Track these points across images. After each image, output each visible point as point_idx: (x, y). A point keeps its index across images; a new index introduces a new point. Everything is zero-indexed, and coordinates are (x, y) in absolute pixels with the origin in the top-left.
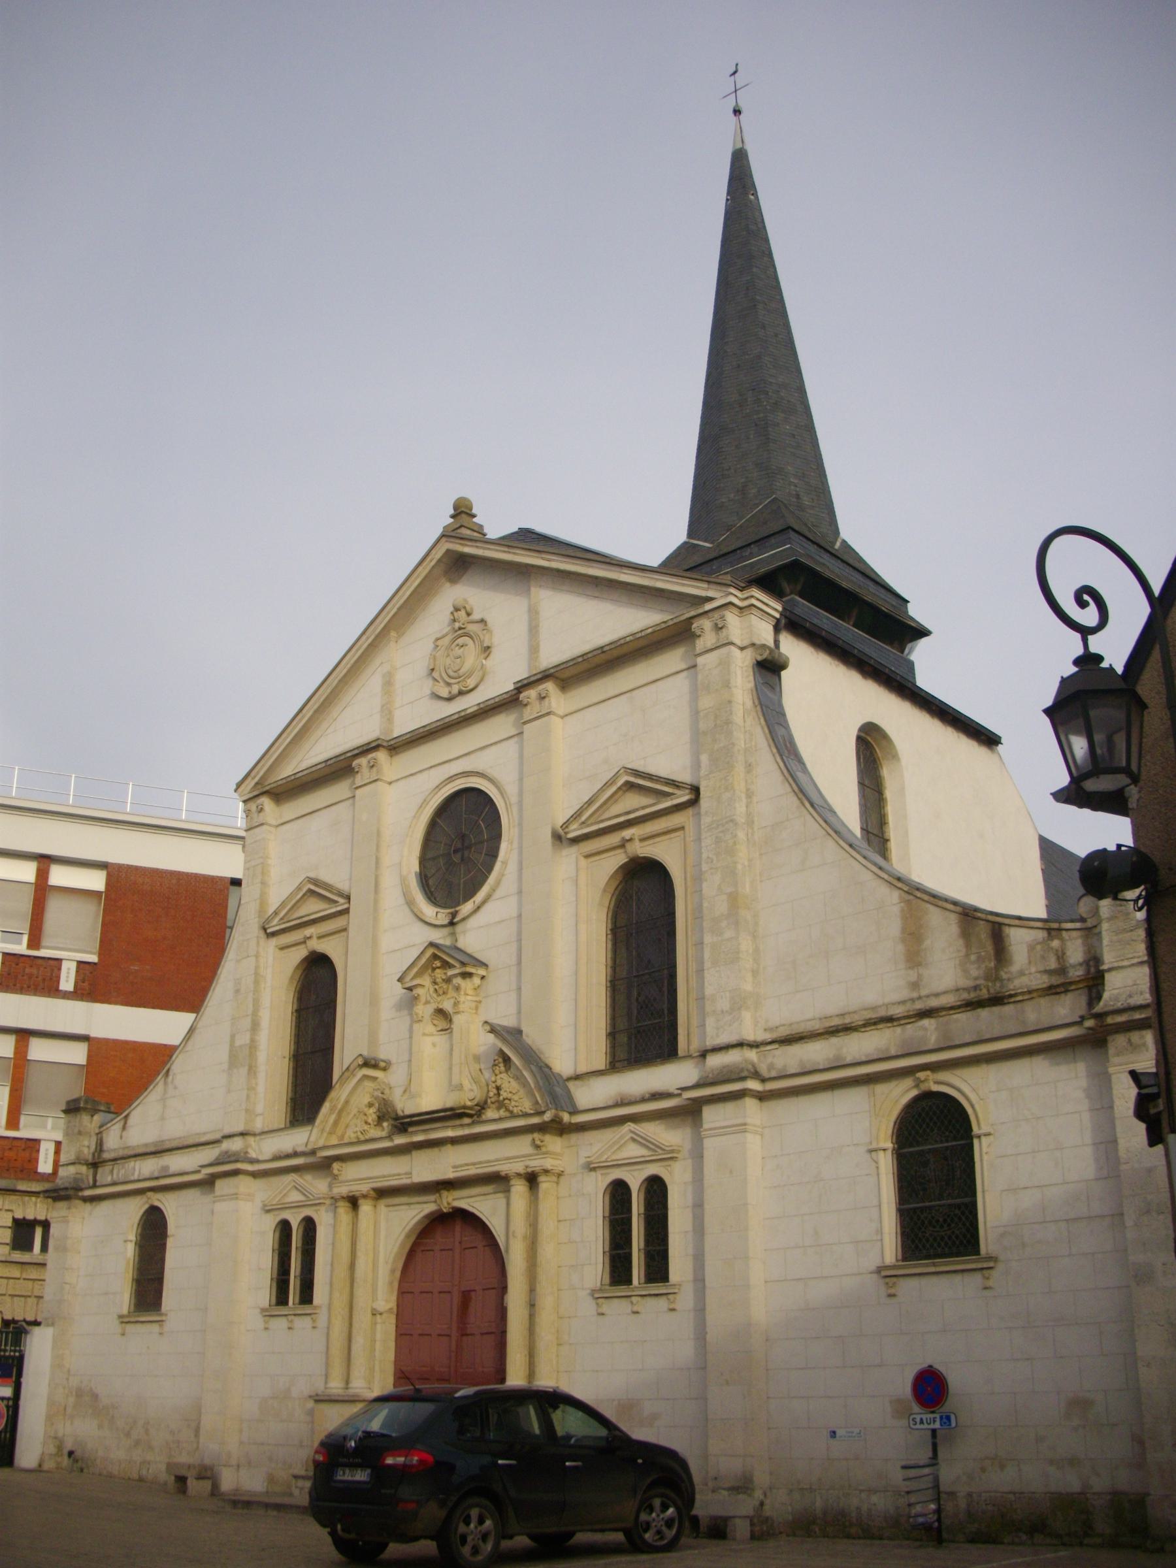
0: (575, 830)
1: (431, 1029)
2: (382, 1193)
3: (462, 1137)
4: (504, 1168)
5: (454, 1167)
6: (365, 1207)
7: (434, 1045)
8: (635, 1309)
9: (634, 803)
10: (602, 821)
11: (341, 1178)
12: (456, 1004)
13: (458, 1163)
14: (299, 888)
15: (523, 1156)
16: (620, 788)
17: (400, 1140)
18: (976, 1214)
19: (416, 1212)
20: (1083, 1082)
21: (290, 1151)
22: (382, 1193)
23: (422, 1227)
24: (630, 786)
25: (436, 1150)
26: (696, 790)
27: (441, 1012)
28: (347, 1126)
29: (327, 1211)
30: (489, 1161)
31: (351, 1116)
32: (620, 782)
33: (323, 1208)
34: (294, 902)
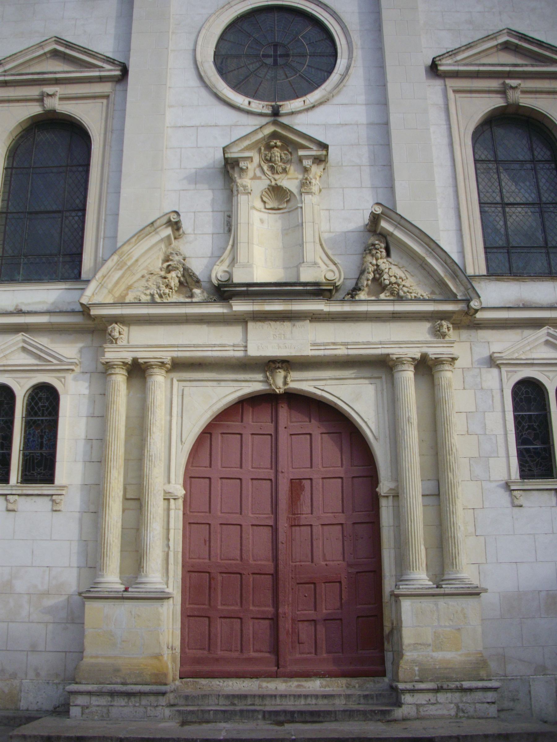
0: (450, 65)
1: (259, 204)
2: (178, 366)
3: (329, 313)
4: (395, 352)
5: (314, 344)
6: (159, 380)
7: (262, 221)
8: (11, 507)
9: (507, 59)
10: (484, 65)
11: (119, 342)
12: (305, 184)
13: (318, 341)
14: (40, 45)
15: (419, 342)
16: (45, 54)
17: (217, 309)
18: (516, 428)
19: (233, 389)
20: (241, 330)
21: (11, 308)
22: (178, 366)
23: (226, 407)
24: (55, 54)
25: (287, 324)
26: (125, 71)
27: (277, 192)
28: (129, 288)
29: (75, 379)
30: (368, 343)
31: (139, 276)
32: (47, 49)
33: (69, 376)
34: (28, 58)
